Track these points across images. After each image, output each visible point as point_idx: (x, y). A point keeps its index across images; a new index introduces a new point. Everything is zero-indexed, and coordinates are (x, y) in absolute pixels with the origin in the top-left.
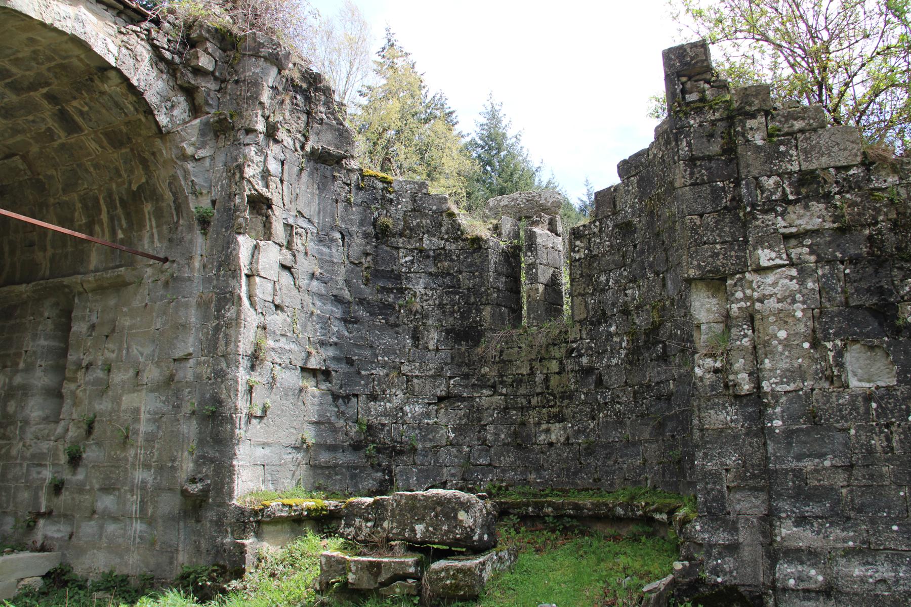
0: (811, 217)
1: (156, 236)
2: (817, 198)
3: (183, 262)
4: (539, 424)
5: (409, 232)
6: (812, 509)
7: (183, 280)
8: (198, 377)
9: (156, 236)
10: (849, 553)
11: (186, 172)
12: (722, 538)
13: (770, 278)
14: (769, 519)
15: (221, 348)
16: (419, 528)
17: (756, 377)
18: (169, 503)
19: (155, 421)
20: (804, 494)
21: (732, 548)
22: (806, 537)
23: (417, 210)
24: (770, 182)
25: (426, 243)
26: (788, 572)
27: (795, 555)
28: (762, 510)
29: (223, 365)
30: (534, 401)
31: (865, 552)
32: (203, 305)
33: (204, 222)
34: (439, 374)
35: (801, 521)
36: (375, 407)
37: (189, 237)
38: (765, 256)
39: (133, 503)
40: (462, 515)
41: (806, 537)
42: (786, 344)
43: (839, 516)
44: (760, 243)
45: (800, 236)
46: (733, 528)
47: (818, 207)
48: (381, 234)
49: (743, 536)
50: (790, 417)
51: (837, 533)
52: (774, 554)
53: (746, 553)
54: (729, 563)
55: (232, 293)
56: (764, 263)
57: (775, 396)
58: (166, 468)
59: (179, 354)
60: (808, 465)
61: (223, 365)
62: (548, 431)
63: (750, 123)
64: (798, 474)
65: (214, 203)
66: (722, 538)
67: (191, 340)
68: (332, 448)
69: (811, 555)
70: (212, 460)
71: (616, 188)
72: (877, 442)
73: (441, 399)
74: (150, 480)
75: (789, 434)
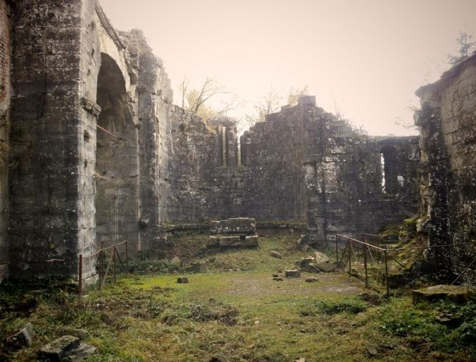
0: (338, 150)
1: (114, 129)
2: (341, 145)
3: (130, 141)
4: (233, 198)
5: (189, 130)
6: (336, 221)
7: (132, 148)
8: (141, 183)
9: (114, 129)
10: (343, 231)
11: (131, 107)
12: (313, 229)
13: (328, 165)
14: (325, 225)
15: (151, 173)
16: (238, 228)
17: (323, 189)
18: (130, 228)
19: (122, 199)
20: (334, 217)
21: (316, 232)
22: (334, 228)
23: (192, 122)
24: (330, 140)
25: (195, 134)
26: (329, 237)
27: (332, 232)
28: (323, 222)
29: (152, 179)
30: (232, 191)
31: (347, 231)
32: (142, 156)
33: (138, 126)
34: (201, 181)
35: (333, 224)
36: (183, 192)
37: (132, 132)
38: (327, 159)
39: (115, 229)
40: (252, 224)
41: (334, 228)
42: (331, 181)
43: (341, 224)
44: (326, 155)
45: (336, 154)
46: (316, 226)
47: (341, 148)
48: (182, 127)
49: (319, 228)
50: (331, 199)
51: (341, 227)
52: (326, 232)
53: (319, 232)
54: (315, 235)
55: (154, 154)
56: (327, 160)
57: (329, 194)
58: (130, 215)
59: (133, 175)
60: (335, 211)
61: (152, 179)
62: (236, 201)
63: (327, 123)
64: (333, 214)
65: (140, 119)
66: (313, 229)
67: (138, 170)
68: (171, 206)
69: (335, 232)
70: (149, 211)
71: (264, 123)
72: (351, 206)
73: (201, 189)
74: (122, 219)
75: (331, 203)
